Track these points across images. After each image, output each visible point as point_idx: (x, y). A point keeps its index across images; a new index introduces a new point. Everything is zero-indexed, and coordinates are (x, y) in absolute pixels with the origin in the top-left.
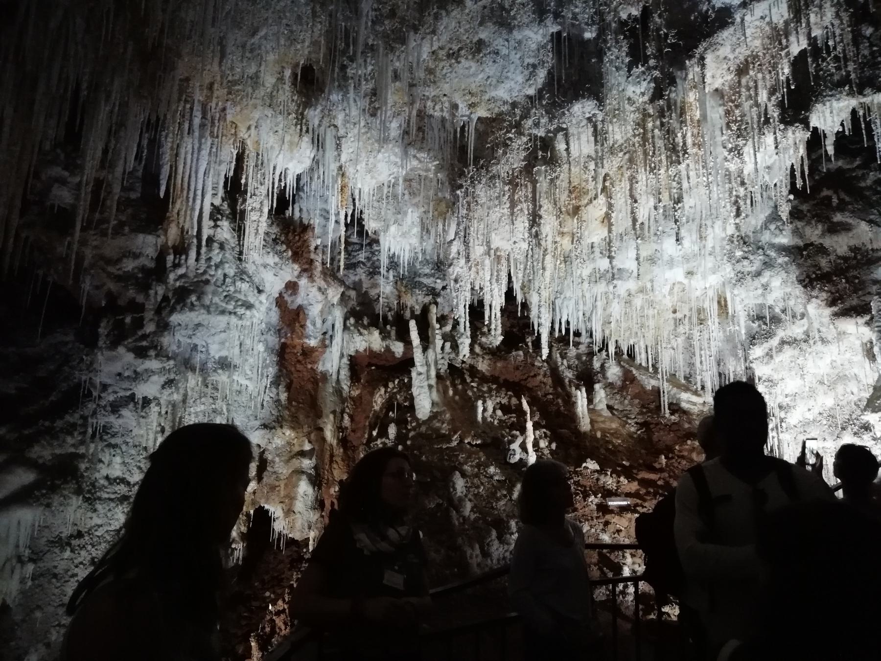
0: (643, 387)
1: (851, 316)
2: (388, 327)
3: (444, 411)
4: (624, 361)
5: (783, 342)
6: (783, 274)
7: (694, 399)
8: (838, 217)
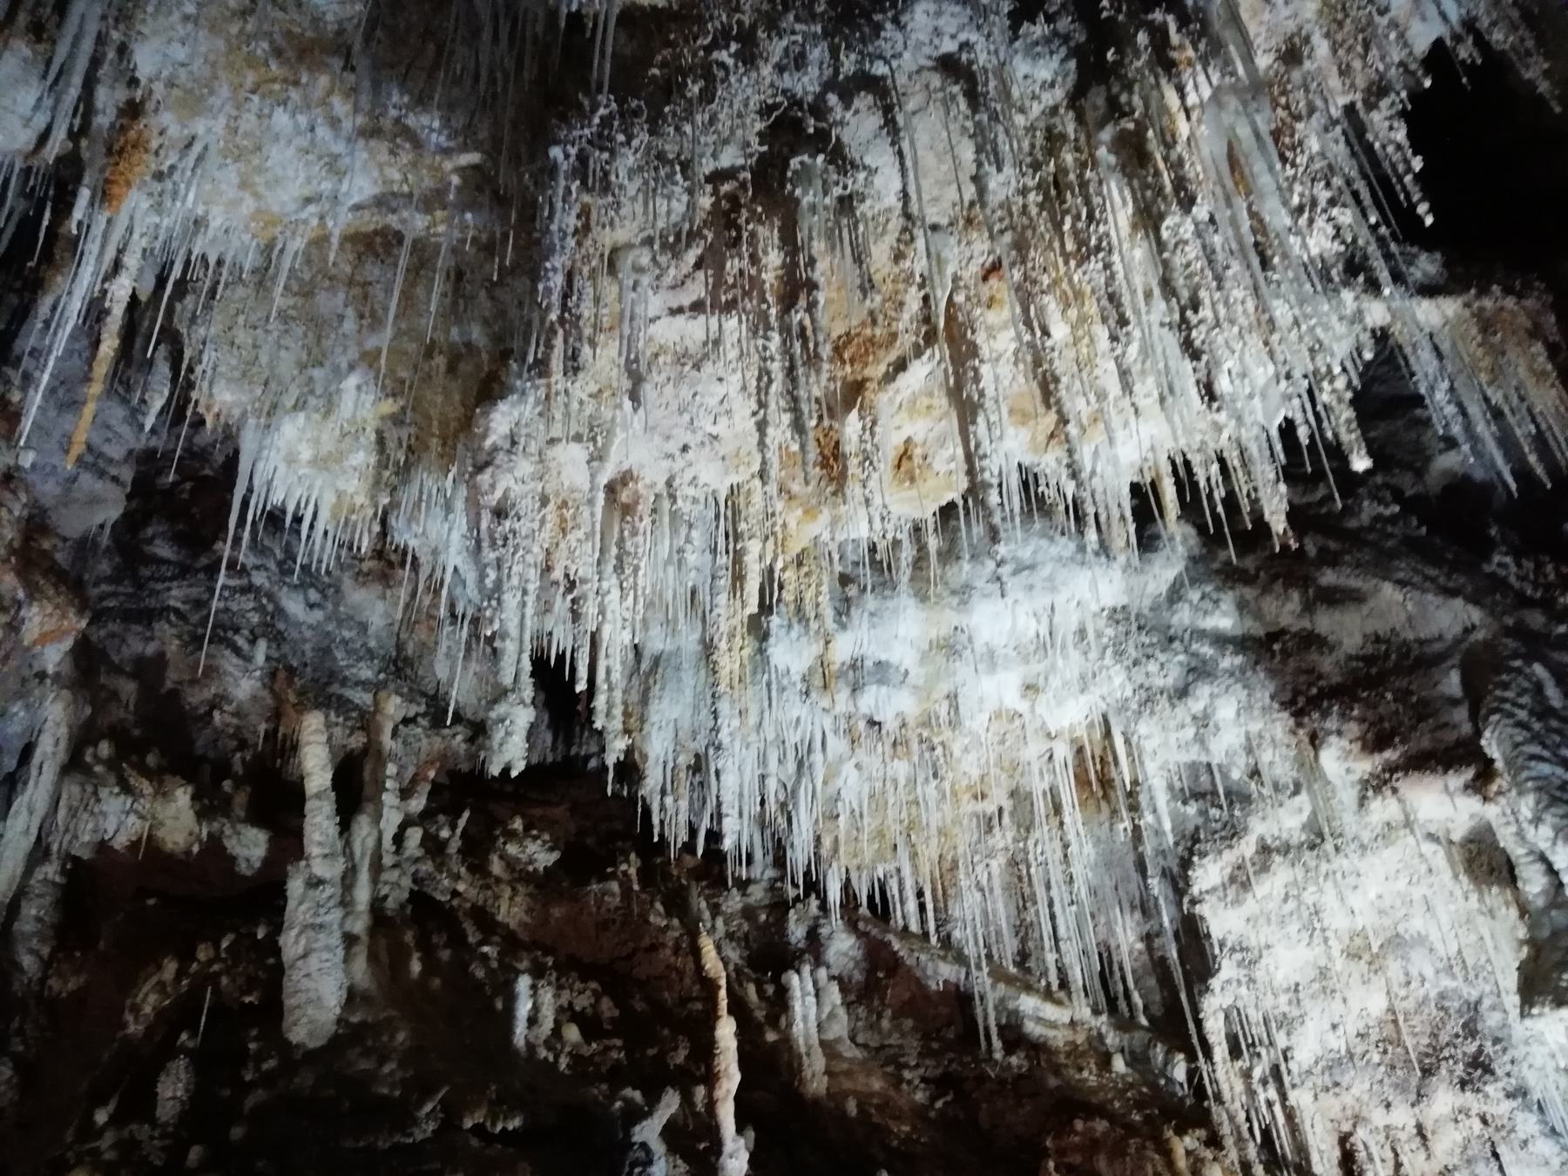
0: (920, 985)
1: (1433, 771)
2: (227, 785)
3: (389, 1020)
4: (866, 920)
5: (1265, 850)
6: (1240, 692)
7: (1050, 1011)
8: (1328, 577)
